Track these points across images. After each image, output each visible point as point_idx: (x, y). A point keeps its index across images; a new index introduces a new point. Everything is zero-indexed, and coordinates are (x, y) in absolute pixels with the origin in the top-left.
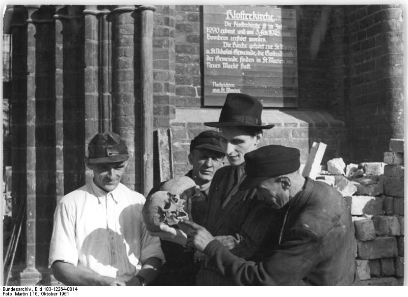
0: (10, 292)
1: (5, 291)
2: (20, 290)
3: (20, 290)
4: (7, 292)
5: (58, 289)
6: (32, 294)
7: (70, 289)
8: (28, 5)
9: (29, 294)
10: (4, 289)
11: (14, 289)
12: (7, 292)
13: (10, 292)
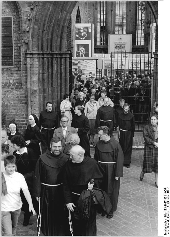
0: (167, 231)
1: (167, 234)
4: (167, 233)
6: (168, 209)
9: (168, 211)
12: (167, 233)
13: (167, 231)
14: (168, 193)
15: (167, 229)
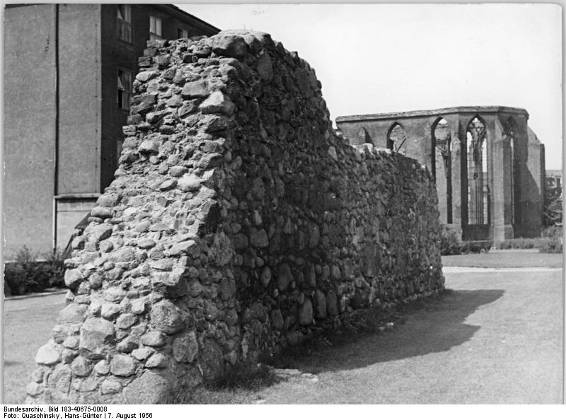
0: (13, 413)
2: (28, 410)
3: (28, 410)
4: (10, 413)
8: (464, 291)
10: (6, 409)
11: (20, 410)
12: (10, 413)
13: (13, 413)
15: (20, 413)
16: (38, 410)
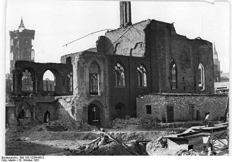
0: (6, 159)
1: (3, 159)
2: (11, 158)
3: (11, 158)
4: (4, 159)
5: (33, 157)
6: (18, 160)
7: (40, 157)
9: (16, 160)
11: (8, 158)
12: (4, 159)
13: (6, 159)
14: (33, 160)
15: (8, 159)
16: (16, 158)
